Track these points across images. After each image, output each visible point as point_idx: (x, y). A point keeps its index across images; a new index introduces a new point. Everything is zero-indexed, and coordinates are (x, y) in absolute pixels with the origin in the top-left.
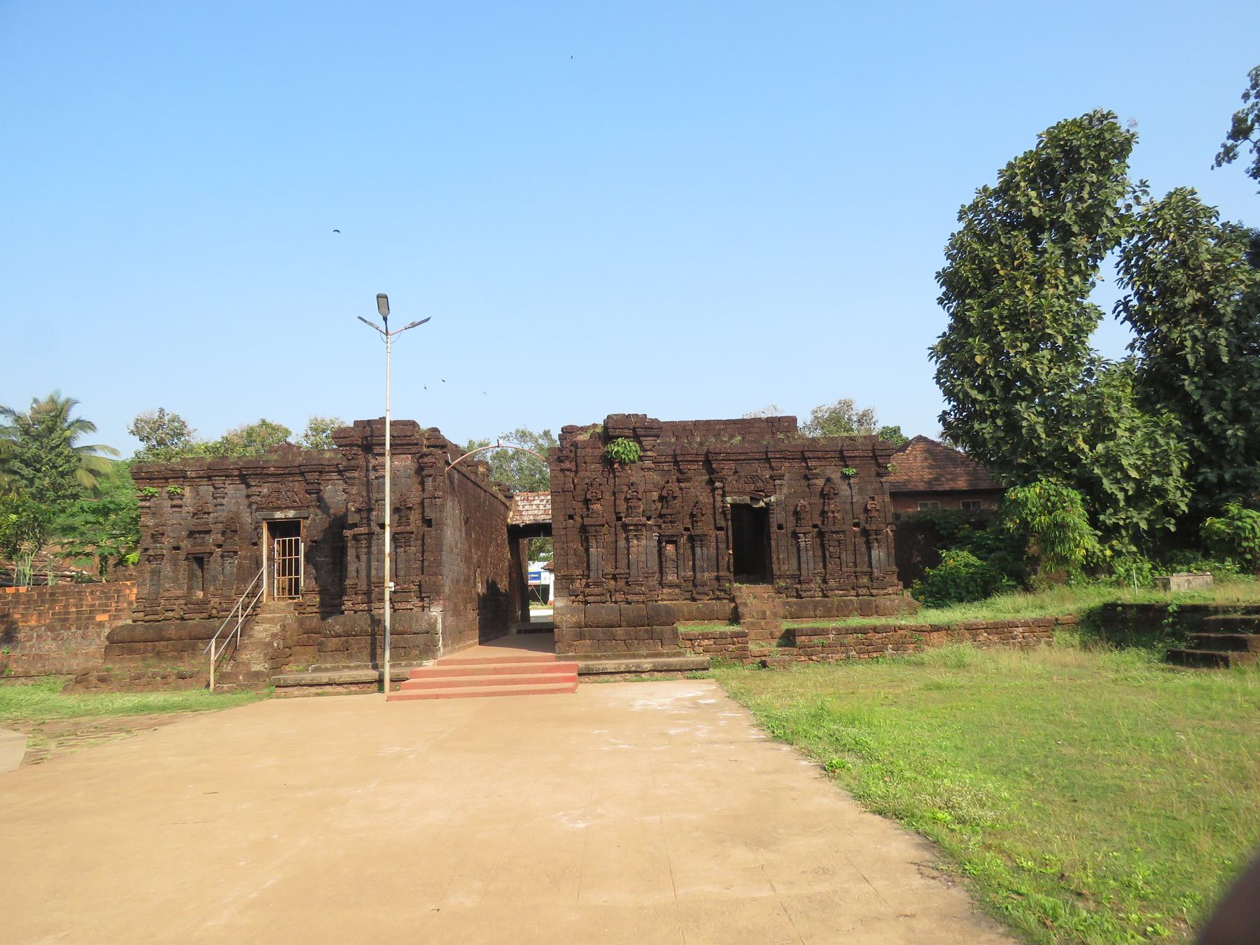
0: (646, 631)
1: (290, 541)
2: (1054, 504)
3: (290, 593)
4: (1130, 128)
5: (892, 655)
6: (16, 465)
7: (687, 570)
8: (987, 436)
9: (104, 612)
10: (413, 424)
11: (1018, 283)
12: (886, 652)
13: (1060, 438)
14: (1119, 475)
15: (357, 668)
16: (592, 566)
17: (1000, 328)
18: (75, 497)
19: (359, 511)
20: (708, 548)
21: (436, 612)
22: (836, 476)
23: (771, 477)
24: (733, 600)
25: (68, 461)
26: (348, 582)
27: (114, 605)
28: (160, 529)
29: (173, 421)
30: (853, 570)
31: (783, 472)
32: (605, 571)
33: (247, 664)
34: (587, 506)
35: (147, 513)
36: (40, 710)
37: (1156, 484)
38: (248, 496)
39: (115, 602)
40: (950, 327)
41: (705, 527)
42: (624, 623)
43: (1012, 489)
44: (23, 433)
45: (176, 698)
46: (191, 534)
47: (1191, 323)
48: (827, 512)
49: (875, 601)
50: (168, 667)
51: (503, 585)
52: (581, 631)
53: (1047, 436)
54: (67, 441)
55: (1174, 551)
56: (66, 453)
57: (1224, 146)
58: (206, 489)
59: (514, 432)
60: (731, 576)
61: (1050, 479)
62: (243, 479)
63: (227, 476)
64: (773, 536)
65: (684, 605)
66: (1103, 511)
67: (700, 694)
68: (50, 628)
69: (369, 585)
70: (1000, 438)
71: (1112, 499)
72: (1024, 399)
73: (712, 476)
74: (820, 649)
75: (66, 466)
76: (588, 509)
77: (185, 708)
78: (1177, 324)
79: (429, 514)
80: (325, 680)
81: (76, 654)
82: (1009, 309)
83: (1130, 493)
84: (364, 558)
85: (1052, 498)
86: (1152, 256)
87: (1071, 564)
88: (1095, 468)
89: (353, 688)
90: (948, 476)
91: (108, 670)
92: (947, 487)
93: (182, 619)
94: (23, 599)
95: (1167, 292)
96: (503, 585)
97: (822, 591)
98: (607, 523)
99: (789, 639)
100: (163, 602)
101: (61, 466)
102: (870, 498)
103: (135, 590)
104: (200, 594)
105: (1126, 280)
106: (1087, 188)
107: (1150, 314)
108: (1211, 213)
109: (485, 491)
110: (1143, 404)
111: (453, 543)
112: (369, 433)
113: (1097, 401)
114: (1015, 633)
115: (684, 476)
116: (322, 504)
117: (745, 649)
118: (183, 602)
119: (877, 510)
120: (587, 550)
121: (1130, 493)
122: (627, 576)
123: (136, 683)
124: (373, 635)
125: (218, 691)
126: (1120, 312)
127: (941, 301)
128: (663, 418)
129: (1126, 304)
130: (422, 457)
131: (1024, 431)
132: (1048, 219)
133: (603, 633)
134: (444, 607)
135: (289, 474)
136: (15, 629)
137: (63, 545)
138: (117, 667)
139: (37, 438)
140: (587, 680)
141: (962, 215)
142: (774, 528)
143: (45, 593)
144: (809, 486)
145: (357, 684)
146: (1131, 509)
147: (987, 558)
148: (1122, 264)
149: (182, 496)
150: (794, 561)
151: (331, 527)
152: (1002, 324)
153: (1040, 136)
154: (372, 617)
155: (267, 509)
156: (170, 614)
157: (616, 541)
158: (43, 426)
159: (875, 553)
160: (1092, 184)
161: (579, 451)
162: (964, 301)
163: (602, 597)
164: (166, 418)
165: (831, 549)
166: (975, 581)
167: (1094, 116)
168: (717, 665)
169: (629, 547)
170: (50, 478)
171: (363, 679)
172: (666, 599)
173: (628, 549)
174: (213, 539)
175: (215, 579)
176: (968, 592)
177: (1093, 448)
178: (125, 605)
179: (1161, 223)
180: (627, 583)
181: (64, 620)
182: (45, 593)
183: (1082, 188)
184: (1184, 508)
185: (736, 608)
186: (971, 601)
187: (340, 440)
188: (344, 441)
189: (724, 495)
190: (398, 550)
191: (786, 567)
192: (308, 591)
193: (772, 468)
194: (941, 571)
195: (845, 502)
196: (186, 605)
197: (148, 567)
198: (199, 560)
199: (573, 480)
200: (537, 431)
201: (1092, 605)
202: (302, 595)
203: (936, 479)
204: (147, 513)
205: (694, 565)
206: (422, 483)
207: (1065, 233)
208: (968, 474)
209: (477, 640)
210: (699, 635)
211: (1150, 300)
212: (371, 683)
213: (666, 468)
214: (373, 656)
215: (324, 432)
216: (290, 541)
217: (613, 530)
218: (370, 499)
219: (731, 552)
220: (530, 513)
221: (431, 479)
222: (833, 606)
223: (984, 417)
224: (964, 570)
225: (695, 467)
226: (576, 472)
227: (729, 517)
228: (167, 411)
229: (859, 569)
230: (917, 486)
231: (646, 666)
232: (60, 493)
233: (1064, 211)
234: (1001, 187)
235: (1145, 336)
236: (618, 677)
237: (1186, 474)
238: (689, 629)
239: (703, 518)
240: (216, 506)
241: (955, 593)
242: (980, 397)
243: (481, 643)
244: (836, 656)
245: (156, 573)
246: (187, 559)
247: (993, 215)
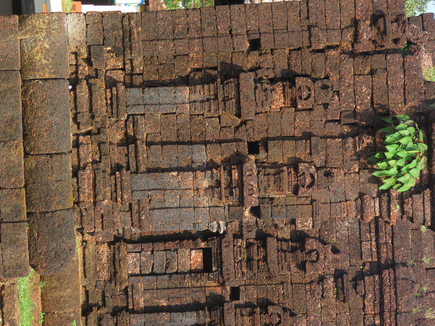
7: (148, 295)
16: (151, 93)
32: (141, 121)
34: (282, 79)
42: (33, 162)
76: (273, 81)
98: (244, 123)
115: (348, 285)
122: (133, 169)
133: (12, 121)
157: (205, 143)
161: (398, 58)
163: (87, 115)
169: (193, 170)
180: (119, 168)
205: (158, 310)
213: (366, 246)
217: (230, 136)
225: (369, 310)
226: (353, 54)
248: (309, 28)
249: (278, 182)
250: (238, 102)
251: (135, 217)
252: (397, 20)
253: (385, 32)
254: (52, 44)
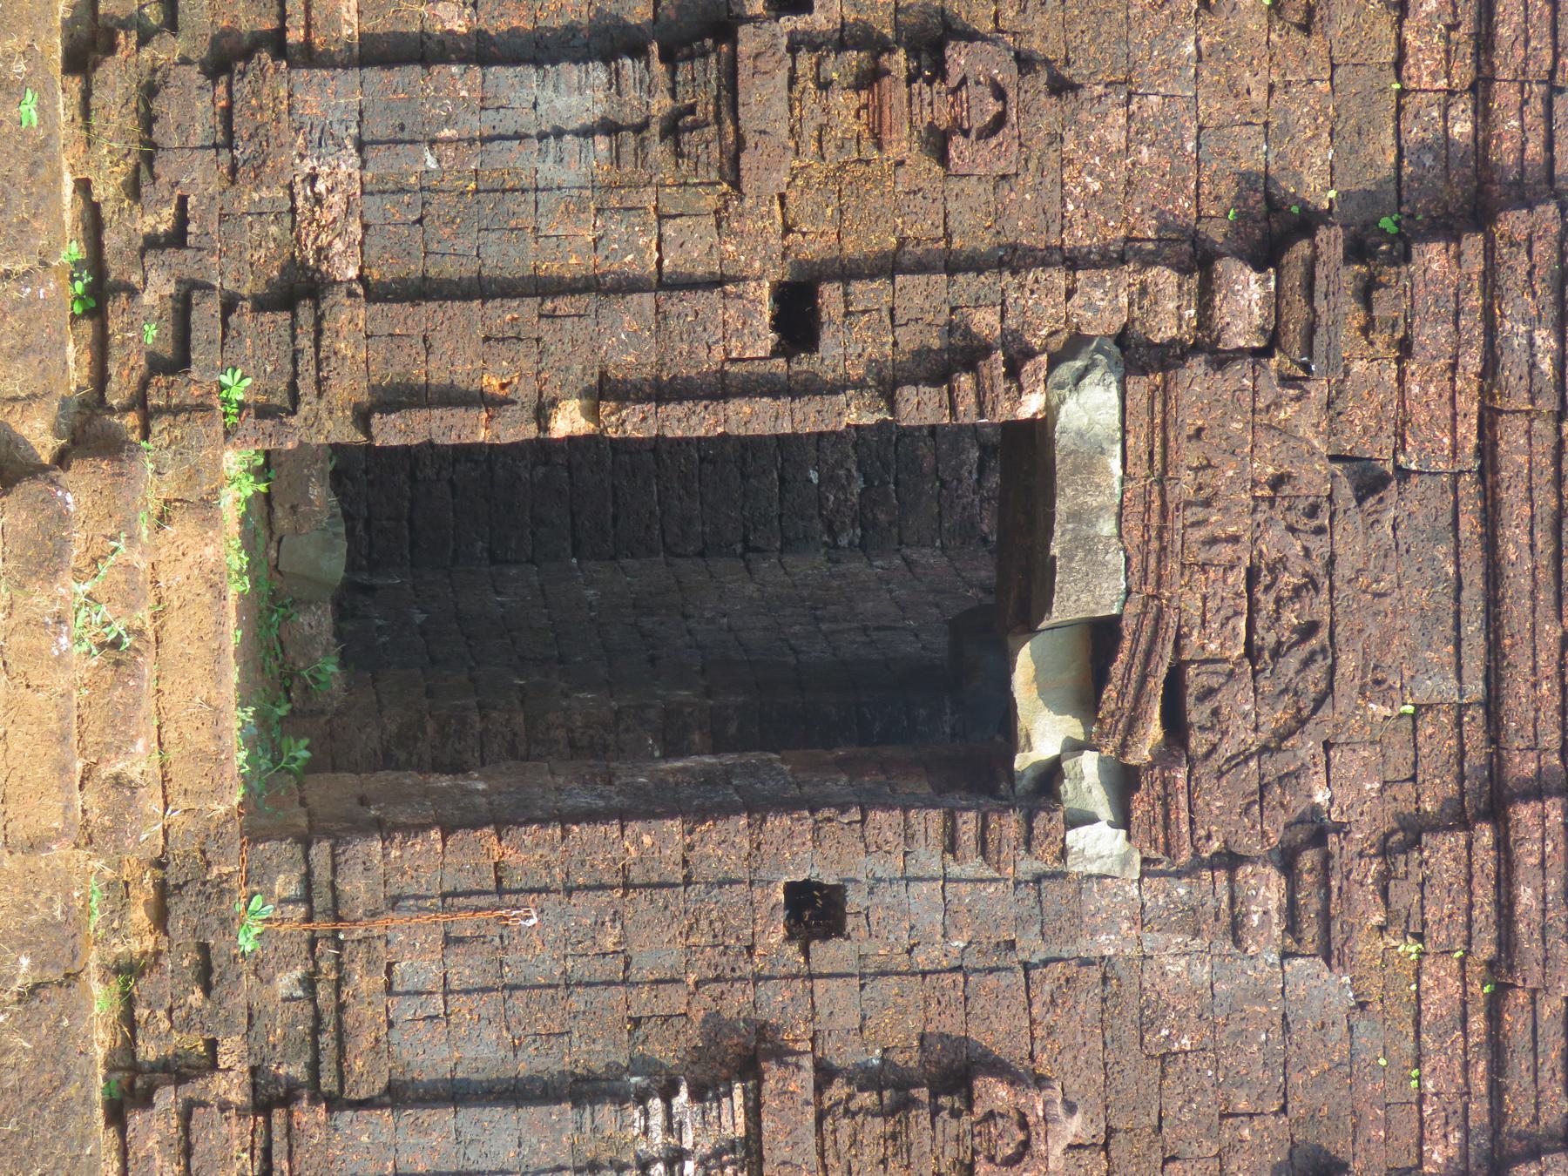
31: (1366, 947)
73: (1330, 241)
219: (568, 421)
225: (1424, 69)
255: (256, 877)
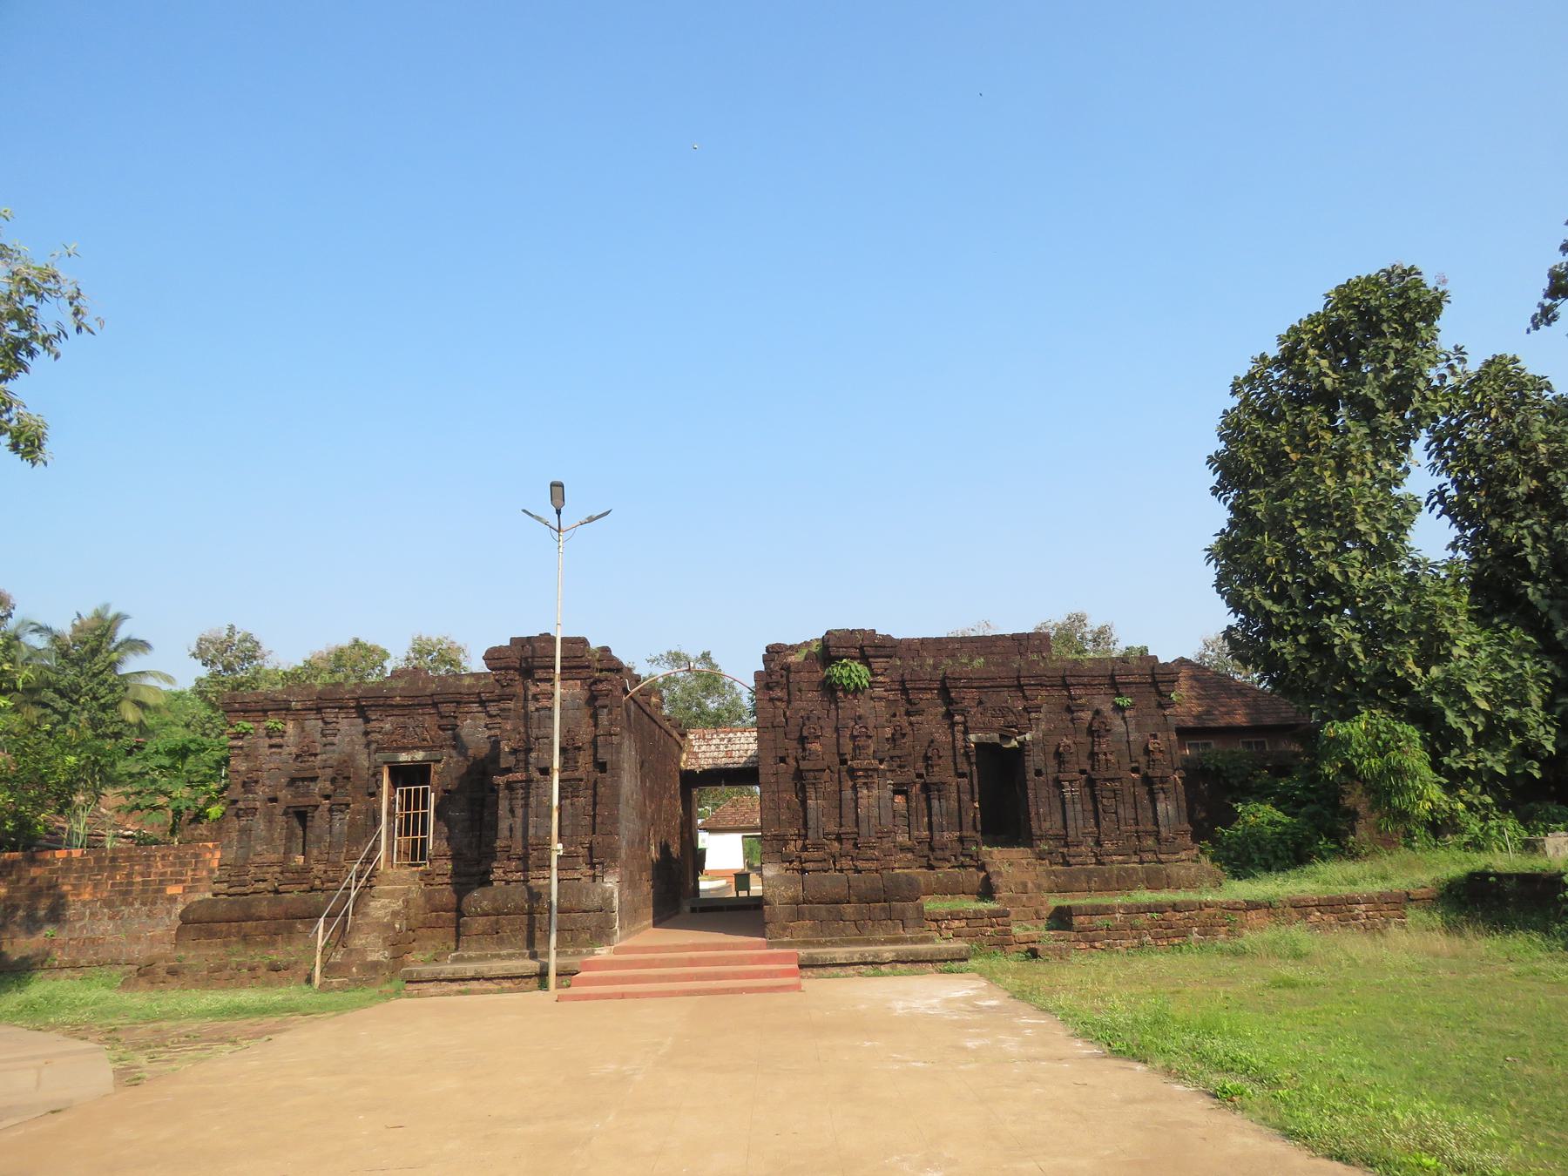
0: (883, 909)
1: (417, 791)
2: (1386, 743)
3: (414, 858)
4: (1439, 286)
5: (1198, 941)
6: (49, 694)
7: (922, 829)
8: (1288, 657)
9: (178, 882)
10: (584, 641)
11: (1316, 469)
12: (1191, 937)
13: (1384, 659)
14: (1464, 706)
15: (510, 957)
16: (811, 824)
17: (1296, 523)
18: (117, 735)
19: (514, 751)
20: (947, 800)
21: (611, 883)
22: (1106, 708)
23: (1025, 709)
24: (982, 867)
25: (112, 691)
26: (499, 843)
27: (190, 873)
28: (254, 775)
29: (245, 641)
30: (1133, 828)
31: (1039, 702)
33: (362, 952)
34: (803, 745)
35: (239, 755)
36: (101, 1012)
37: (1513, 716)
38: (366, 733)
39: (193, 870)
40: (1231, 523)
41: (943, 773)
42: (854, 899)
43: (1329, 723)
44: (60, 656)
45: (276, 996)
46: (293, 781)
47: (1528, 516)
48: (1097, 754)
49: (1165, 869)
50: (258, 956)
51: (675, 850)
52: (799, 907)
53: (1366, 657)
54: (112, 666)
55: (1532, 804)
56: (110, 680)
57: (1541, 305)
58: (314, 724)
59: (665, 653)
60: (978, 837)
61: (1374, 711)
62: (361, 711)
63: (340, 708)
64: (1030, 785)
65: (918, 873)
66: (1447, 752)
67: (971, 993)
68: (108, 903)
69: (525, 847)
70: (1305, 660)
71: (1458, 736)
72: (1331, 611)
73: (951, 708)
74: (1104, 933)
75: (110, 697)
76: (804, 750)
77: (292, 1010)
78: (1509, 518)
79: (603, 755)
80: (470, 974)
81: (139, 938)
82: (1306, 501)
83: (1480, 728)
84: (519, 812)
85: (1383, 736)
86: (1470, 437)
87: (1412, 820)
88: (1434, 697)
89: (507, 984)
90: (1222, 709)
91: (180, 960)
92: (1222, 723)
93: (276, 892)
94: (76, 865)
95: (1494, 482)
96: (675, 850)
97: (1096, 855)
98: (829, 768)
99: (1061, 919)
100: (252, 869)
101: (103, 697)
102: (1151, 735)
103: (218, 855)
104: (300, 859)
105: (1439, 465)
106: (1392, 356)
107: (1475, 506)
108: (1541, 384)
109: (660, 727)
110: (1481, 617)
111: (629, 793)
112: (530, 653)
113: (1427, 613)
114: (1356, 911)
115: (914, 708)
116: (458, 744)
117: (1007, 933)
118: (277, 869)
119: (1161, 751)
120: (804, 803)
121: (1480, 728)
122: (856, 836)
123: (217, 976)
124: (531, 913)
125: (324, 988)
126: (1434, 504)
127: (1215, 491)
128: (898, 635)
129: (1441, 494)
130: (595, 683)
131: (1337, 651)
132: (1345, 393)
133: (829, 911)
134: (621, 876)
135: (418, 705)
136: (63, 905)
137: (128, 796)
138: (191, 955)
139: (76, 662)
140: (809, 974)
141: (1235, 388)
142: (1031, 775)
143: (105, 858)
144: (1072, 720)
145: (511, 978)
146: (1482, 749)
147: (1297, 814)
148: (1433, 447)
149: (283, 734)
150: (1058, 817)
151: (469, 773)
152: (1298, 518)
153: (1327, 296)
154: (530, 889)
155: (388, 749)
156: (262, 885)
157: (841, 791)
158: (87, 647)
159: (1161, 807)
160: (1397, 351)
162: (1245, 491)
163: (824, 864)
164: (237, 637)
165: (1105, 801)
166: (1284, 842)
167: (1393, 271)
168: (977, 955)
169: (857, 798)
170: (89, 711)
171: (520, 971)
172: (904, 868)
173: (856, 801)
174: (320, 789)
175: (320, 839)
176: (1276, 857)
177: (1426, 672)
178: (204, 873)
179: (1479, 397)
180: (855, 845)
181: (125, 893)
182: (105, 858)
183: (1386, 356)
184: (1550, 747)
185: (987, 878)
186: (1283, 869)
187: (493, 662)
188: (498, 664)
189: (966, 732)
190: (563, 802)
191: (1047, 825)
192: (438, 856)
193: (1025, 697)
194: (1237, 830)
195: (1120, 741)
196: (282, 873)
197: (236, 824)
198: (302, 816)
199: (785, 714)
200: (694, 652)
201: (1451, 875)
202: (430, 861)
203: (1208, 713)
204: (239, 755)
206: (595, 716)
207: (1365, 410)
208: (1247, 705)
209: (651, 921)
210: (948, 914)
211: (1472, 488)
212: (530, 977)
214: (530, 942)
215: (429, 653)
216: (417, 791)
218: (528, 737)
219: (977, 805)
220: (708, 754)
221: (605, 710)
222: (1111, 877)
223: (1282, 633)
224: (1269, 830)
225: (929, 696)
226: (789, 702)
227: (973, 760)
228: (237, 629)
229: (1141, 828)
230: (1183, 720)
231: (886, 955)
232: (99, 731)
233: (1364, 384)
234: (1283, 355)
235: (1468, 533)
236: (850, 970)
237: (1548, 706)
238: (947, 905)
239: (940, 762)
240: (325, 745)
241: (1260, 859)
242: (1276, 609)
243: (655, 925)
244: (1126, 943)
245: (245, 831)
246: (285, 813)
247: (1274, 388)
248: (773, 727)
249: (864, 747)
250: (817, 771)
251: (885, 835)
252: (770, 676)
253: (777, 683)
254: (782, 885)
255: (1038, 846)
